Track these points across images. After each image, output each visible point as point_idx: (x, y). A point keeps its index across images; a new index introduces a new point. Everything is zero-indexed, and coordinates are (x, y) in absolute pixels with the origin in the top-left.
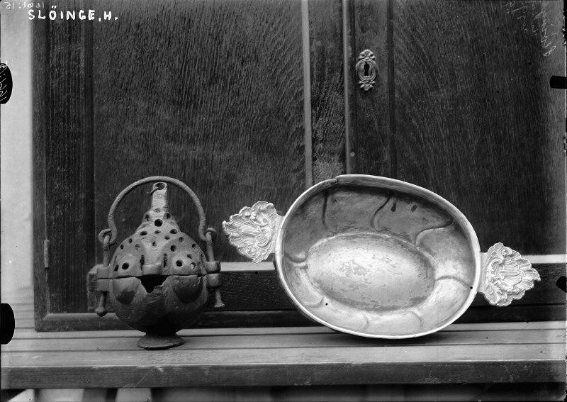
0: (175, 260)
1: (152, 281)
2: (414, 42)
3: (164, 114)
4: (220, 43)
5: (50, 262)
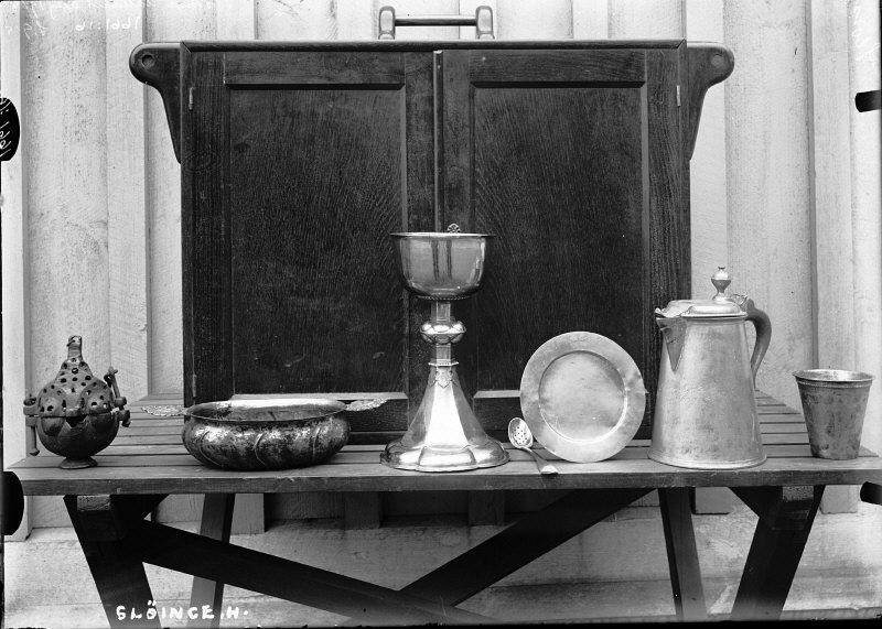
0: (91, 401)
1: (75, 420)
2: (492, 216)
3: (289, 273)
4: (335, 215)
5: (197, 393)
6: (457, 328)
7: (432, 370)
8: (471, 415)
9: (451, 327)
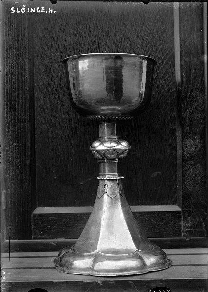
6: (123, 145)
7: (101, 183)
8: (135, 224)
9: (119, 143)
